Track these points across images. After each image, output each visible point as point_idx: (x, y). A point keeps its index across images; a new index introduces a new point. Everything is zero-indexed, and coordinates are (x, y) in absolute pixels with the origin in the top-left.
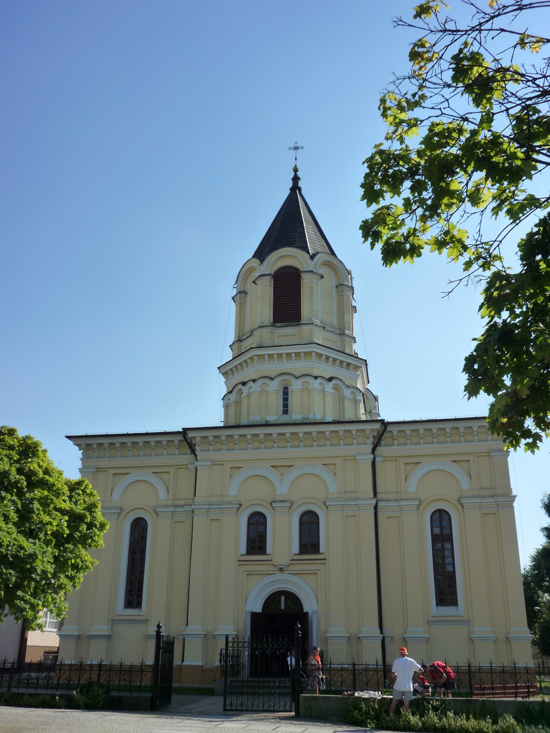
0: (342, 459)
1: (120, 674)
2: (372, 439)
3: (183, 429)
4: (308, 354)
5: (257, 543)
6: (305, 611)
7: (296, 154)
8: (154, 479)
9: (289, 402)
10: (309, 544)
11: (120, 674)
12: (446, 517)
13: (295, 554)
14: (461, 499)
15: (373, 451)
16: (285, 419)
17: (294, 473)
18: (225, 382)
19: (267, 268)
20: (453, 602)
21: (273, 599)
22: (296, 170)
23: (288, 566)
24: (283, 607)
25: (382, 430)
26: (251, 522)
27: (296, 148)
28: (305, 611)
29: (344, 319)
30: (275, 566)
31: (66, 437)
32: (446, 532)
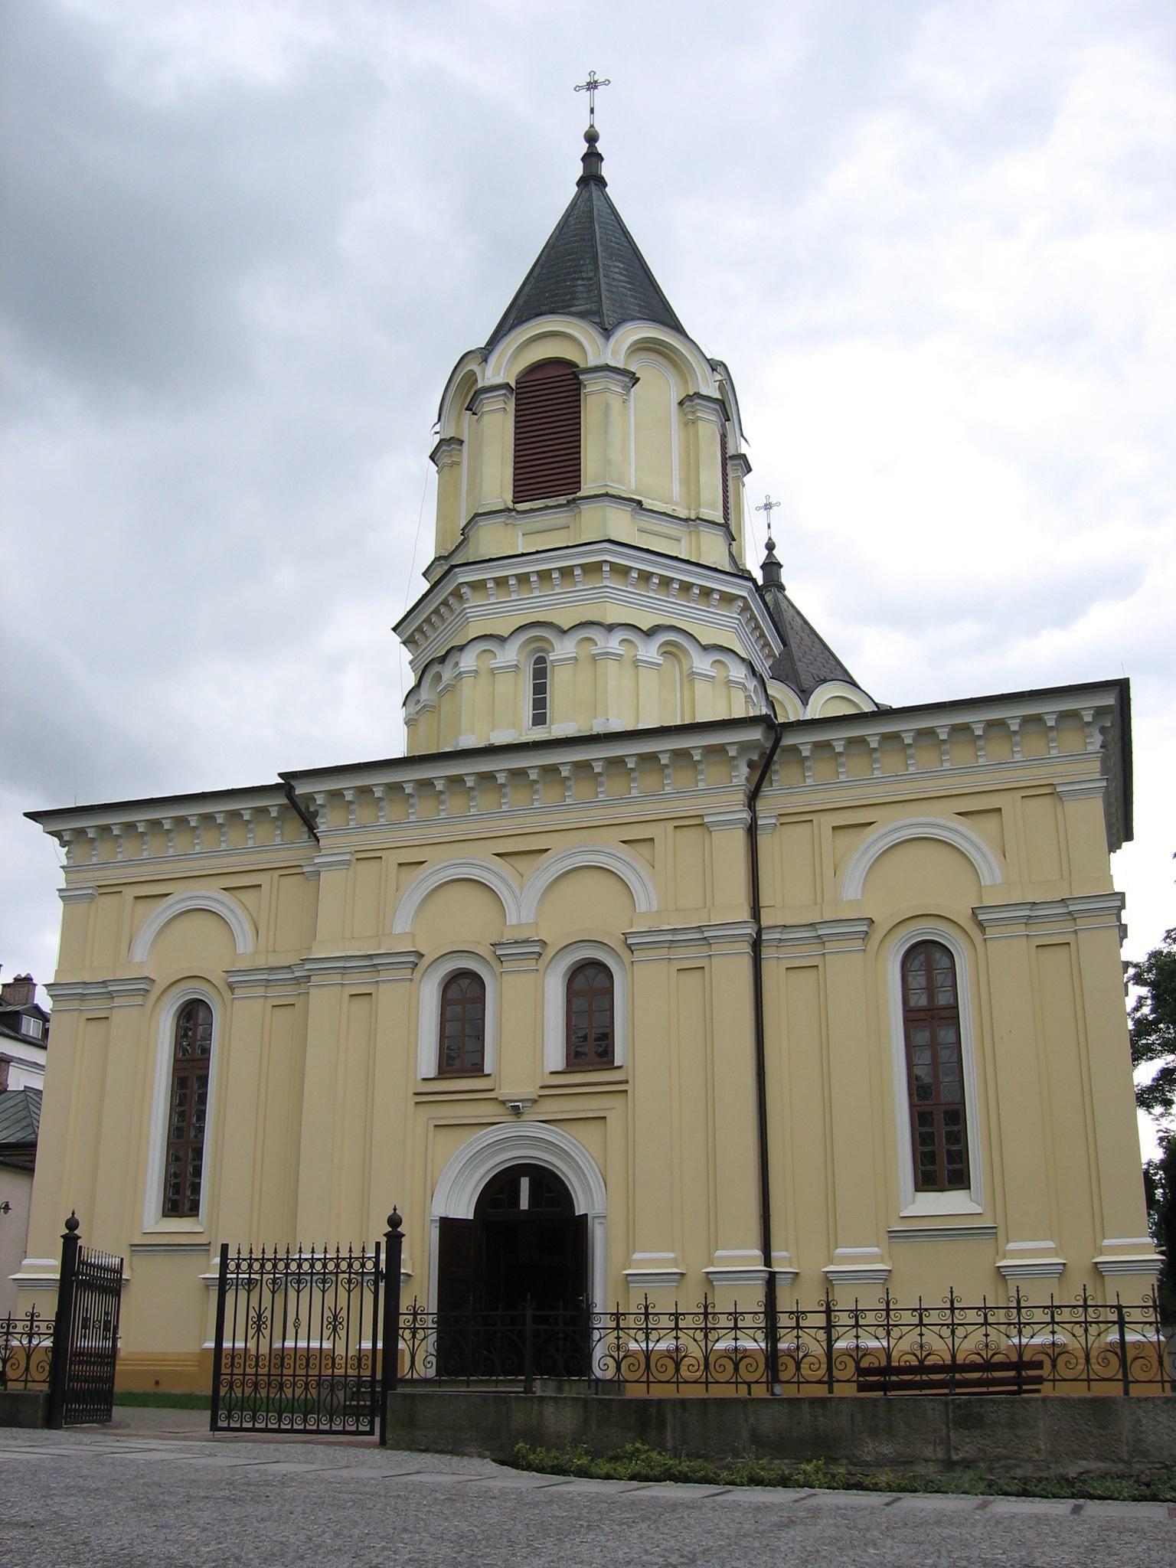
0: (671, 824)
1: (414, 1337)
2: (745, 770)
3: (281, 775)
4: (592, 569)
5: (461, 1051)
6: (579, 1211)
7: (592, 99)
8: (228, 905)
9: (548, 695)
10: (591, 1044)
11: (414, 1337)
12: (945, 962)
13: (552, 1073)
14: (977, 912)
15: (753, 798)
16: (539, 734)
17: (550, 868)
18: (411, 663)
19: (499, 369)
20: (193, 1210)
21: (498, 1191)
22: (591, 138)
23: (535, 1101)
24: (524, 1205)
25: (769, 745)
26: (449, 996)
27: (592, 86)
28: (579, 1211)
29: (698, 481)
30: (503, 1102)
31: (26, 815)
32: (943, 999)
